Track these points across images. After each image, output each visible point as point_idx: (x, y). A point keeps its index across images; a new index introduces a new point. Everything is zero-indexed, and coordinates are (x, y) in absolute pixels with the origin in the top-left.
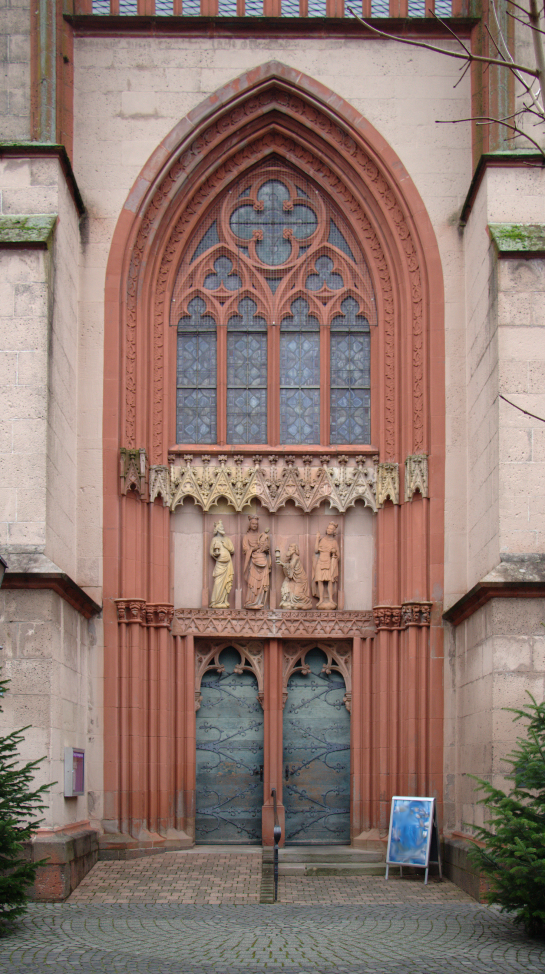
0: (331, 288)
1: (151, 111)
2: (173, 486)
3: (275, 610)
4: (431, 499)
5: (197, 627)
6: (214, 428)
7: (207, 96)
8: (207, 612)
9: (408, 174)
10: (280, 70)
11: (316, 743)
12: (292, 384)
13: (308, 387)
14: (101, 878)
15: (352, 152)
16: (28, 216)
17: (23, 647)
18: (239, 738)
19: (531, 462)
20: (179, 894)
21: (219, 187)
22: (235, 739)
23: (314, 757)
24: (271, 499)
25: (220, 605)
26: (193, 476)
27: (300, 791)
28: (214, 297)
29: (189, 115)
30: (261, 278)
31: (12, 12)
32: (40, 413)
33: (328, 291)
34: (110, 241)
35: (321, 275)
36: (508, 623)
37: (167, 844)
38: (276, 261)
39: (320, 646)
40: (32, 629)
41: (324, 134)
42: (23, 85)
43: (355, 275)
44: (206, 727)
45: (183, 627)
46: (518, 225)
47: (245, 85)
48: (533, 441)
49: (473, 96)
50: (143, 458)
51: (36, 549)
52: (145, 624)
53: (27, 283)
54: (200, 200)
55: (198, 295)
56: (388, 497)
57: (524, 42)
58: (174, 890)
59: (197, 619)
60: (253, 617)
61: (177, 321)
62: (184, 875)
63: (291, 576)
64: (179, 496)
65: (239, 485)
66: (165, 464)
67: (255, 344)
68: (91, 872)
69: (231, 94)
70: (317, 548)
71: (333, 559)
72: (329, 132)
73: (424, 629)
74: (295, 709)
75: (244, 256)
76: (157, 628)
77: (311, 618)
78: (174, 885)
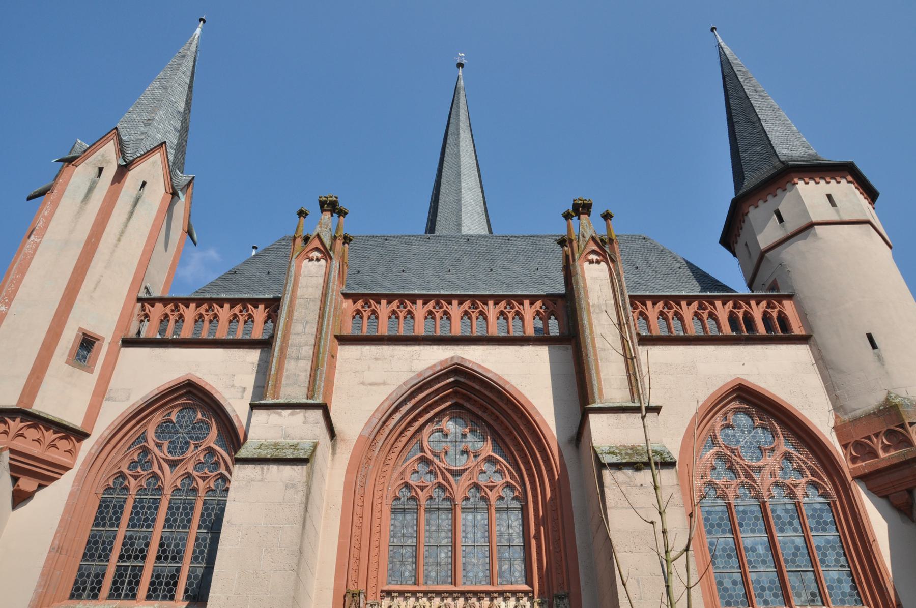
0: (495, 480)
1: (381, 381)
6: (416, 572)
9: (540, 414)
10: (460, 360)
12: (470, 543)
13: (480, 545)
16: (299, 441)
19: (642, 601)
21: (422, 421)
28: (417, 486)
29: (404, 383)
31: (305, 336)
32: (292, 567)
33: (493, 483)
34: (350, 453)
35: (488, 472)
38: (457, 464)
41: (487, 393)
42: (306, 371)
43: (510, 473)
46: (612, 445)
47: (439, 368)
48: (641, 586)
49: (576, 373)
50: (362, 596)
53: (294, 482)
54: (409, 429)
55: (407, 485)
57: (602, 349)
66: (378, 600)
67: (444, 516)
69: (430, 372)
75: (436, 461)
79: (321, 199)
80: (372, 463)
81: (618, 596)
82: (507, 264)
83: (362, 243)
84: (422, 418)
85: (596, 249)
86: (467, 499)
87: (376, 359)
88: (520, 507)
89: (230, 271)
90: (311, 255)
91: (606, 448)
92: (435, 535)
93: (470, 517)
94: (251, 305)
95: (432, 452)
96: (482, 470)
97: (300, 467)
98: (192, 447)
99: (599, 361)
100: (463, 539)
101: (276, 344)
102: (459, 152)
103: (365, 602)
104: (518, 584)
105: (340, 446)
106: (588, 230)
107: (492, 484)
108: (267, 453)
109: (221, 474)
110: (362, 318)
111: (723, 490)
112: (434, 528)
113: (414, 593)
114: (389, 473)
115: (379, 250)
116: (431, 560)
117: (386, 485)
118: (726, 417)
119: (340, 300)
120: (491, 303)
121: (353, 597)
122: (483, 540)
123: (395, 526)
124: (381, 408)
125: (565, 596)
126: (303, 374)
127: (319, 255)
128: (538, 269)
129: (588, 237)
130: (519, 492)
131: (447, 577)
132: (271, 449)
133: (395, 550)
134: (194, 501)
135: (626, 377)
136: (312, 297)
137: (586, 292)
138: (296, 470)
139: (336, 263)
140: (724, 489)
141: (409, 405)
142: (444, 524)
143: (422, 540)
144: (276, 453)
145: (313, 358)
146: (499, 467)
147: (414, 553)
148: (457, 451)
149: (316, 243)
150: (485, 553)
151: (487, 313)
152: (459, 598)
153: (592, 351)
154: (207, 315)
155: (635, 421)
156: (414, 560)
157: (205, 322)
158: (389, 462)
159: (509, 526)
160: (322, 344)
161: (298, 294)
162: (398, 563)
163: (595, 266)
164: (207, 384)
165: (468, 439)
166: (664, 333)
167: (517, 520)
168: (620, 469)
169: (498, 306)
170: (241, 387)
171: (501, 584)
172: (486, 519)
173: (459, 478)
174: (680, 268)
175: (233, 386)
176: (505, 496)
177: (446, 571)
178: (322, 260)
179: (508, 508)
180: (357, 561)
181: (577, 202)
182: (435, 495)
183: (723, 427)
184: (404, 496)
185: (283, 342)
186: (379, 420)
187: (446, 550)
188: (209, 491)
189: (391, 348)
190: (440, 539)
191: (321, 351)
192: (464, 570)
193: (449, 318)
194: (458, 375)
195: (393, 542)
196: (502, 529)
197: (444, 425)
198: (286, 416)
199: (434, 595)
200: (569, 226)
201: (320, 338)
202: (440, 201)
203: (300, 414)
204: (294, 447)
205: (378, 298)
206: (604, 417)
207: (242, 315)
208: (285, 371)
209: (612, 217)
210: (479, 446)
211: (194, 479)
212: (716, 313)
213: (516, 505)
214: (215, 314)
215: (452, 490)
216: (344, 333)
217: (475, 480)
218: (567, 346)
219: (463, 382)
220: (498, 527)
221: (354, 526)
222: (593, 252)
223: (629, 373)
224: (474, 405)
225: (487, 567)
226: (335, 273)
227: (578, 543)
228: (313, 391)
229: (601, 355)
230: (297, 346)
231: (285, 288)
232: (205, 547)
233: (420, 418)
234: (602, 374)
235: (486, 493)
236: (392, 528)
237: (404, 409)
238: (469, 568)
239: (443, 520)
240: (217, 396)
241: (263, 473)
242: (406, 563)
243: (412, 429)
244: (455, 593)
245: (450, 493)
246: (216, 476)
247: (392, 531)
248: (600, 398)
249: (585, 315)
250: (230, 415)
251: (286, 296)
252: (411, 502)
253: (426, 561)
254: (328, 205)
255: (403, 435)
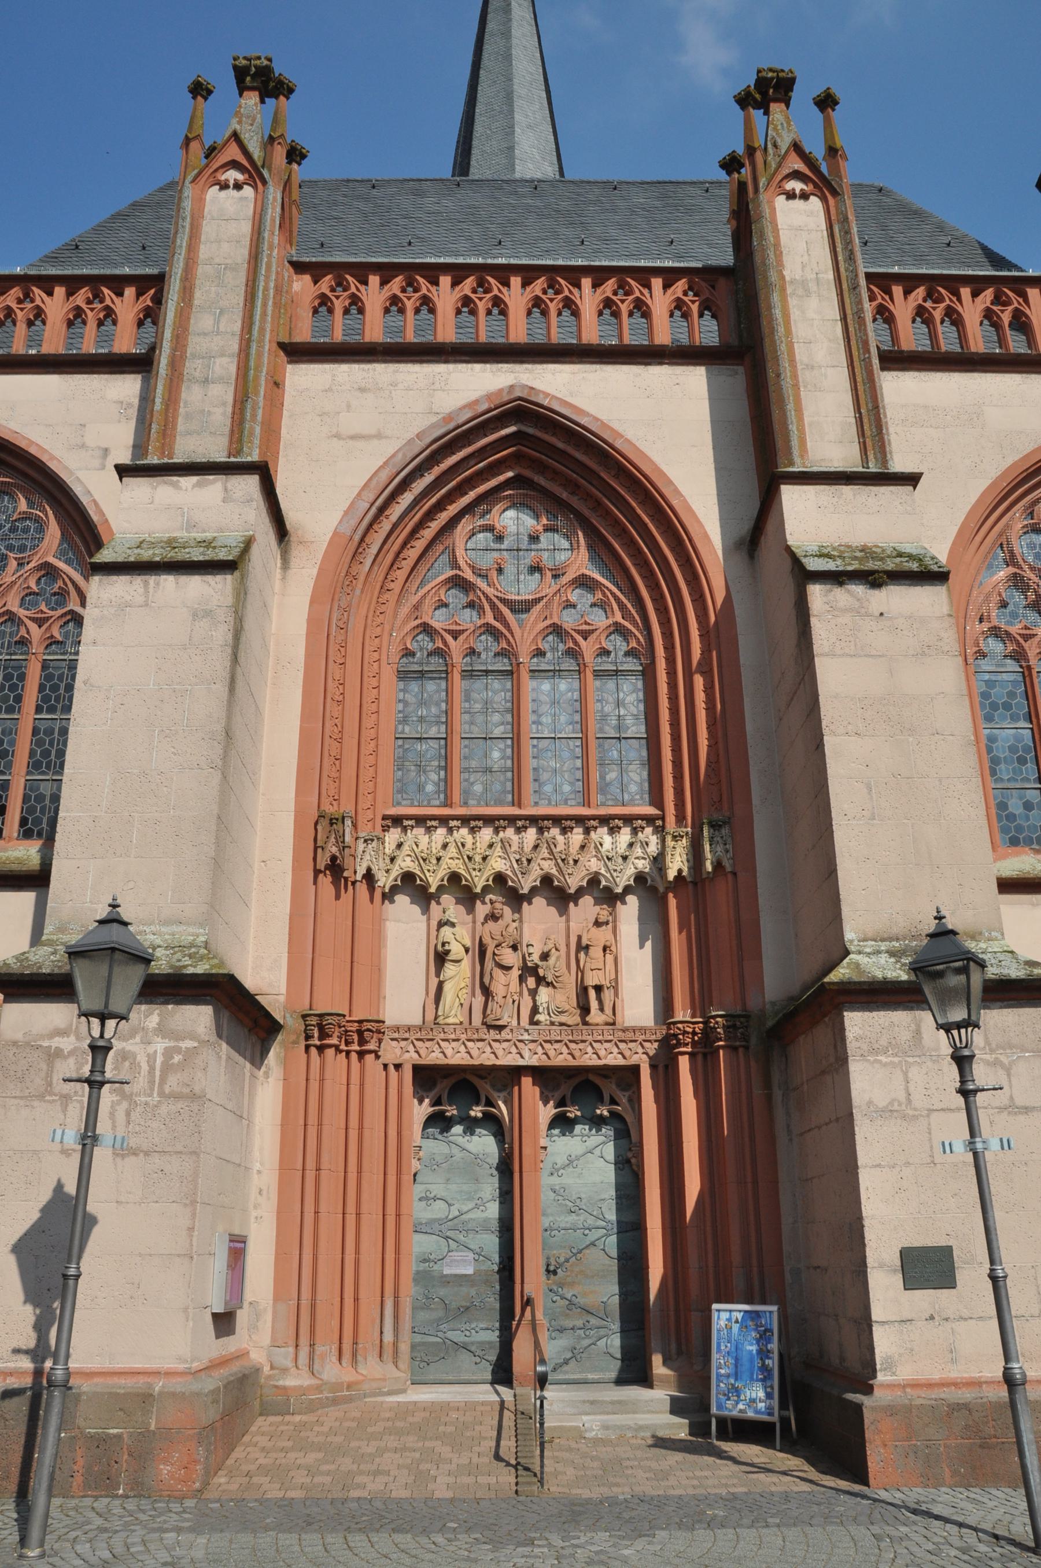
1: (373, 432)
2: (388, 861)
3: (527, 1027)
4: (739, 874)
5: (417, 1052)
7: (440, 417)
8: (432, 1029)
9: (682, 496)
10: (526, 392)
11: (591, 1221)
14: (263, 1449)
15: (613, 473)
16: (215, 535)
17: (163, 1080)
18: (476, 1215)
20: (385, 1479)
21: (453, 509)
22: (470, 1215)
23: (588, 1243)
24: (520, 876)
25: (451, 1020)
26: (415, 847)
27: (569, 1296)
28: (445, 630)
29: (418, 436)
30: (506, 611)
33: (589, 624)
34: (317, 566)
36: (868, 1040)
37: (366, 1387)
39: (592, 1077)
40: (180, 1054)
41: (578, 455)
42: (224, 404)
43: (622, 607)
44: (427, 1199)
45: (398, 1051)
47: (485, 406)
50: (348, 822)
51: (194, 940)
52: (343, 1047)
53: (209, 607)
55: (427, 629)
56: (680, 871)
58: (377, 1473)
59: (417, 1040)
60: (498, 1037)
61: (398, 657)
62: (392, 1442)
63: (550, 979)
64: (396, 872)
65: (478, 858)
66: (378, 832)
67: (496, 685)
68: (246, 1438)
69: (469, 415)
70: (584, 942)
71: (607, 956)
72: (585, 453)
73: (741, 1050)
74: (558, 1170)
76: (361, 1054)
77: (580, 1038)
78: (377, 1460)
79: (237, 63)
80: (360, 586)
81: (830, 812)
82: (613, 232)
83: (326, 192)
84: (454, 505)
85: (801, 170)
86: (540, 653)
87: (362, 390)
88: (641, 668)
89: (67, 244)
90: (223, 178)
91: (813, 548)
92: (480, 719)
93: (546, 686)
94: (108, 288)
95: (473, 568)
96: (568, 600)
97: (219, 578)
98: (14, 564)
99: (802, 389)
100: (534, 726)
101: (160, 352)
102: (509, 48)
103: (355, 835)
104: (634, 805)
105: (297, 553)
106: (784, 134)
107: (587, 627)
108: (154, 554)
109: (71, 612)
110: (331, 311)
111: (1018, 644)
112: (478, 706)
113: (444, 820)
114: (392, 604)
115: (361, 205)
116: (474, 764)
117: (387, 627)
118: (1032, 513)
119: (286, 275)
120: (586, 282)
121: (331, 824)
122: (571, 727)
123: (406, 703)
124: (374, 482)
125: (725, 823)
126: (219, 411)
127: (241, 177)
128: (672, 242)
129: (784, 144)
130: (638, 642)
131: (504, 792)
132: (162, 547)
133: (406, 746)
134: (24, 663)
135: (854, 420)
136: (229, 261)
137: (779, 255)
138: (212, 583)
139: (274, 193)
140: (1021, 641)
141: (428, 478)
142: (497, 699)
143: (456, 726)
144: (172, 554)
145: (237, 379)
146: (600, 596)
147: (443, 752)
148: (522, 566)
149: (233, 152)
150: (573, 751)
151: (578, 302)
152: (526, 828)
153: (788, 368)
154: (22, 309)
155: (870, 499)
156: (443, 764)
157: (18, 324)
158: (392, 585)
159: (618, 704)
160: (253, 350)
161: (201, 255)
162: (413, 768)
163: (798, 203)
164: (32, 442)
165: (541, 546)
166: (923, 345)
167: (633, 692)
168: (841, 584)
169: (599, 290)
170: (99, 448)
171: (603, 804)
172: (575, 690)
173: (524, 616)
174: (949, 245)
175: (83, 446)
176: (611, 648)
177: (501, 783)
178: (245, 187)
179: (617, 671)
180: (337, 762)
181: (764, 74)
182: (479, 647)
183: (1025, 530)
184: (421, 649)
185: (174, 349)
186: (372, 505)
187: (502, 746)
188: (51, 644)
189: (392, 367)
190: (489, 725)
191: (252, 364)
192: (535, 780)
193: (503, 313)
194: (522, 422)
195: (403, 732)
196: (606, 709)
197: (496, 520)
198: (190, 489)
199: (480, 823)
200: (748, 123)
201: (249, 341)
202: (475, 152)
203: (215, 486)
204: (207, 544)
205: (362, 271)
206: (809, 491)
207: (92, 310)
208: (182, 405)
209: (836, 103)
210: (563, 558)
211: (21, 622)
212: (1028, 312)
213: (632, 664)
214: (38, 307)
215: (513, 636)
216: (297, 339)
217: (556, 620)
218: (735, 367)
219: (532, 436)
220: (599, 704)
221: (329, 699)
222: (796, 175)
223: (860, 413)
224: (552, 479)
225: (579, 775)
226: (274, 212)
227: (749, 727)
228: (240, 440)
229: (804, 376)
230: (203, 358)
231: (174, 242)
232: (51, 744)
233: (450, 504)
234: (806, 413)
235: (576, 643)
236: (400, 706)
237: (419, 485)
238: (544, 776)
239: (495, 692)
240: (53, 465)
241: (147, 591)
242: (428, 768)
243: (435, 526)
244: (520, 820)
245: (509, 643)
246: (62, 616)
247: (400, 712)
248: (802, 456)
249: (776, 298)
250: (82, 499)
251: (175, 259)
252: (433, 660)
253: (465, 764)
254: (254, 77)
255: (418, 536)
